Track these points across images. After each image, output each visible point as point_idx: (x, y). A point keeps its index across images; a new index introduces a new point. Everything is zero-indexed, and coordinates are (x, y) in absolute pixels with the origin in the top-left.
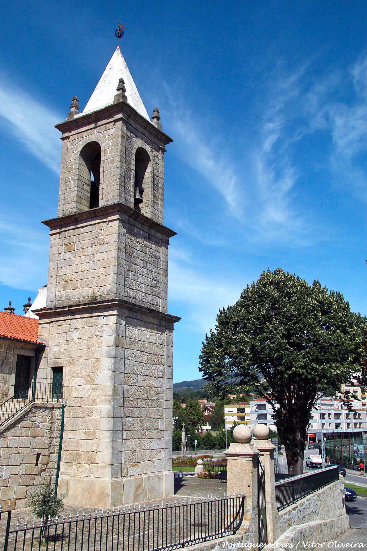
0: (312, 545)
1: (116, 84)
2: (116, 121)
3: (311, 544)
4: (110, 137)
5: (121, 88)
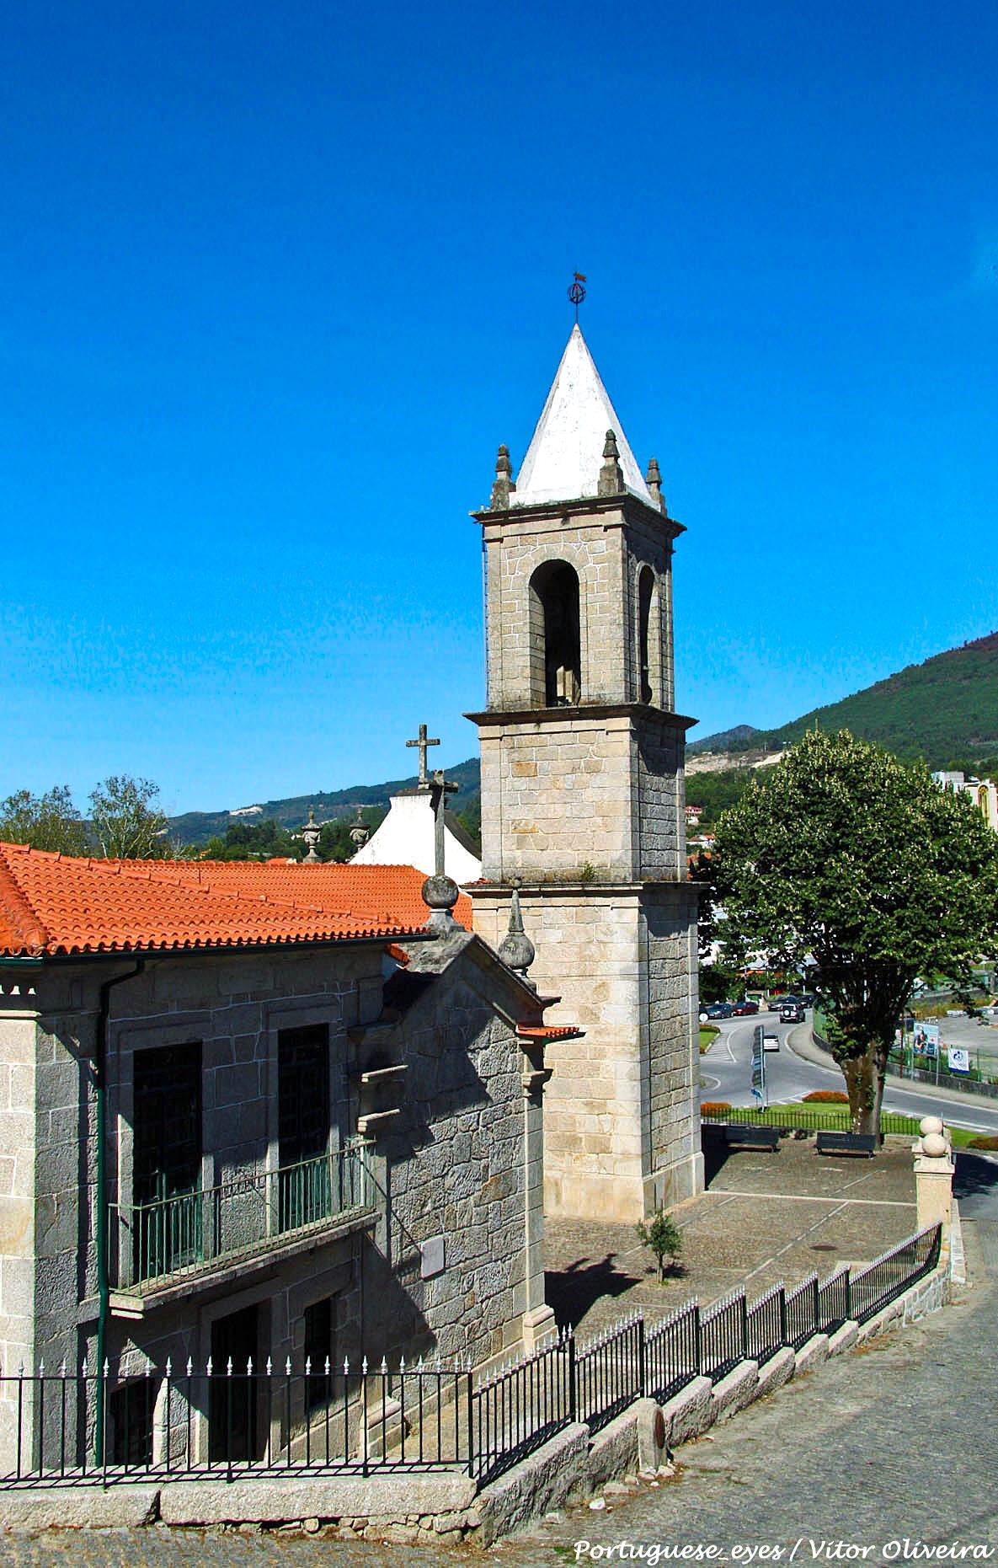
0: (837, 1552)
1: (602, 441)
3: (834, 1549)
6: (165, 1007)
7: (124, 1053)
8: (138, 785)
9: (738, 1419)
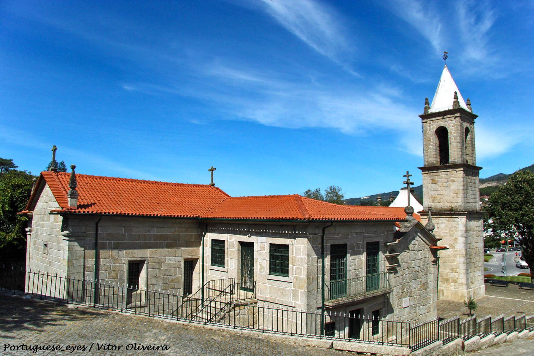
1: (454, 94)
2: (455, 117)
4: (453, 125)
5: (456, 97)
6: (338, 235)
7: (328, 245)
8: (337, 188)
9: (488, 349)
